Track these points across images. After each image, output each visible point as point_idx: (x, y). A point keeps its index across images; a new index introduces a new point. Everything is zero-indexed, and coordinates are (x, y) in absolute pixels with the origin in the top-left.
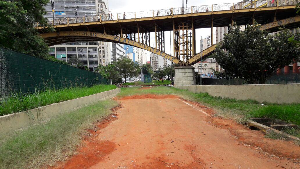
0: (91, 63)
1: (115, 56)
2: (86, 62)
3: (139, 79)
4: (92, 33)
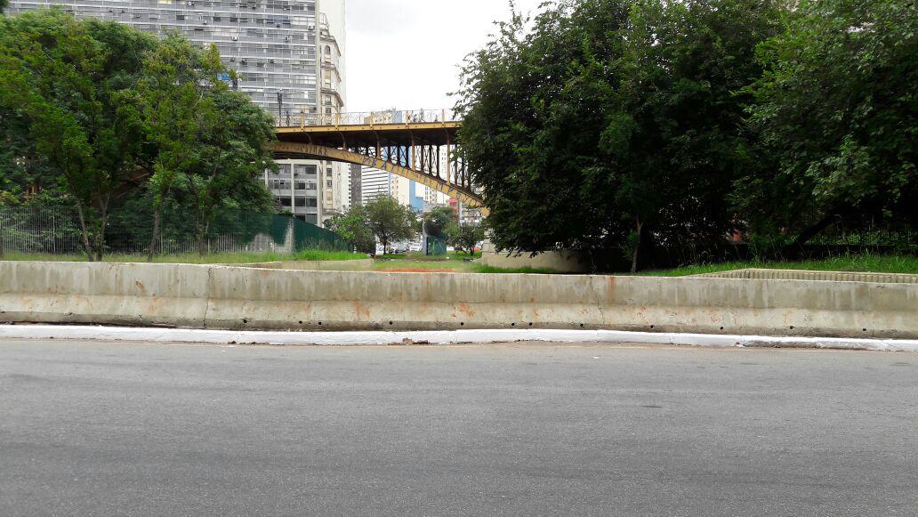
0: (300, 202)
1: (358, 180)
2: (287, 201)
3: (418, 245)
4: (318, 148)
